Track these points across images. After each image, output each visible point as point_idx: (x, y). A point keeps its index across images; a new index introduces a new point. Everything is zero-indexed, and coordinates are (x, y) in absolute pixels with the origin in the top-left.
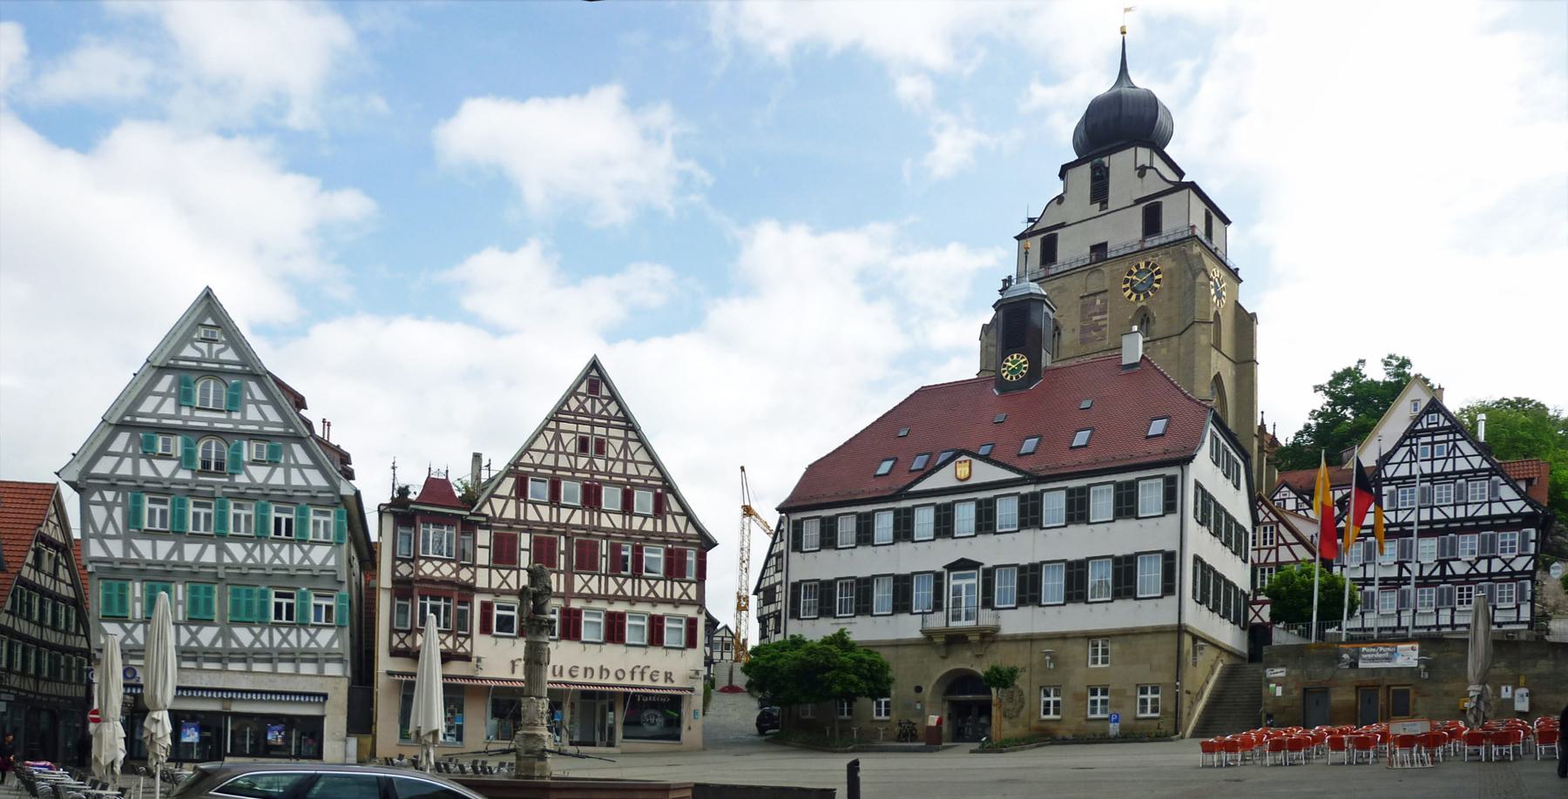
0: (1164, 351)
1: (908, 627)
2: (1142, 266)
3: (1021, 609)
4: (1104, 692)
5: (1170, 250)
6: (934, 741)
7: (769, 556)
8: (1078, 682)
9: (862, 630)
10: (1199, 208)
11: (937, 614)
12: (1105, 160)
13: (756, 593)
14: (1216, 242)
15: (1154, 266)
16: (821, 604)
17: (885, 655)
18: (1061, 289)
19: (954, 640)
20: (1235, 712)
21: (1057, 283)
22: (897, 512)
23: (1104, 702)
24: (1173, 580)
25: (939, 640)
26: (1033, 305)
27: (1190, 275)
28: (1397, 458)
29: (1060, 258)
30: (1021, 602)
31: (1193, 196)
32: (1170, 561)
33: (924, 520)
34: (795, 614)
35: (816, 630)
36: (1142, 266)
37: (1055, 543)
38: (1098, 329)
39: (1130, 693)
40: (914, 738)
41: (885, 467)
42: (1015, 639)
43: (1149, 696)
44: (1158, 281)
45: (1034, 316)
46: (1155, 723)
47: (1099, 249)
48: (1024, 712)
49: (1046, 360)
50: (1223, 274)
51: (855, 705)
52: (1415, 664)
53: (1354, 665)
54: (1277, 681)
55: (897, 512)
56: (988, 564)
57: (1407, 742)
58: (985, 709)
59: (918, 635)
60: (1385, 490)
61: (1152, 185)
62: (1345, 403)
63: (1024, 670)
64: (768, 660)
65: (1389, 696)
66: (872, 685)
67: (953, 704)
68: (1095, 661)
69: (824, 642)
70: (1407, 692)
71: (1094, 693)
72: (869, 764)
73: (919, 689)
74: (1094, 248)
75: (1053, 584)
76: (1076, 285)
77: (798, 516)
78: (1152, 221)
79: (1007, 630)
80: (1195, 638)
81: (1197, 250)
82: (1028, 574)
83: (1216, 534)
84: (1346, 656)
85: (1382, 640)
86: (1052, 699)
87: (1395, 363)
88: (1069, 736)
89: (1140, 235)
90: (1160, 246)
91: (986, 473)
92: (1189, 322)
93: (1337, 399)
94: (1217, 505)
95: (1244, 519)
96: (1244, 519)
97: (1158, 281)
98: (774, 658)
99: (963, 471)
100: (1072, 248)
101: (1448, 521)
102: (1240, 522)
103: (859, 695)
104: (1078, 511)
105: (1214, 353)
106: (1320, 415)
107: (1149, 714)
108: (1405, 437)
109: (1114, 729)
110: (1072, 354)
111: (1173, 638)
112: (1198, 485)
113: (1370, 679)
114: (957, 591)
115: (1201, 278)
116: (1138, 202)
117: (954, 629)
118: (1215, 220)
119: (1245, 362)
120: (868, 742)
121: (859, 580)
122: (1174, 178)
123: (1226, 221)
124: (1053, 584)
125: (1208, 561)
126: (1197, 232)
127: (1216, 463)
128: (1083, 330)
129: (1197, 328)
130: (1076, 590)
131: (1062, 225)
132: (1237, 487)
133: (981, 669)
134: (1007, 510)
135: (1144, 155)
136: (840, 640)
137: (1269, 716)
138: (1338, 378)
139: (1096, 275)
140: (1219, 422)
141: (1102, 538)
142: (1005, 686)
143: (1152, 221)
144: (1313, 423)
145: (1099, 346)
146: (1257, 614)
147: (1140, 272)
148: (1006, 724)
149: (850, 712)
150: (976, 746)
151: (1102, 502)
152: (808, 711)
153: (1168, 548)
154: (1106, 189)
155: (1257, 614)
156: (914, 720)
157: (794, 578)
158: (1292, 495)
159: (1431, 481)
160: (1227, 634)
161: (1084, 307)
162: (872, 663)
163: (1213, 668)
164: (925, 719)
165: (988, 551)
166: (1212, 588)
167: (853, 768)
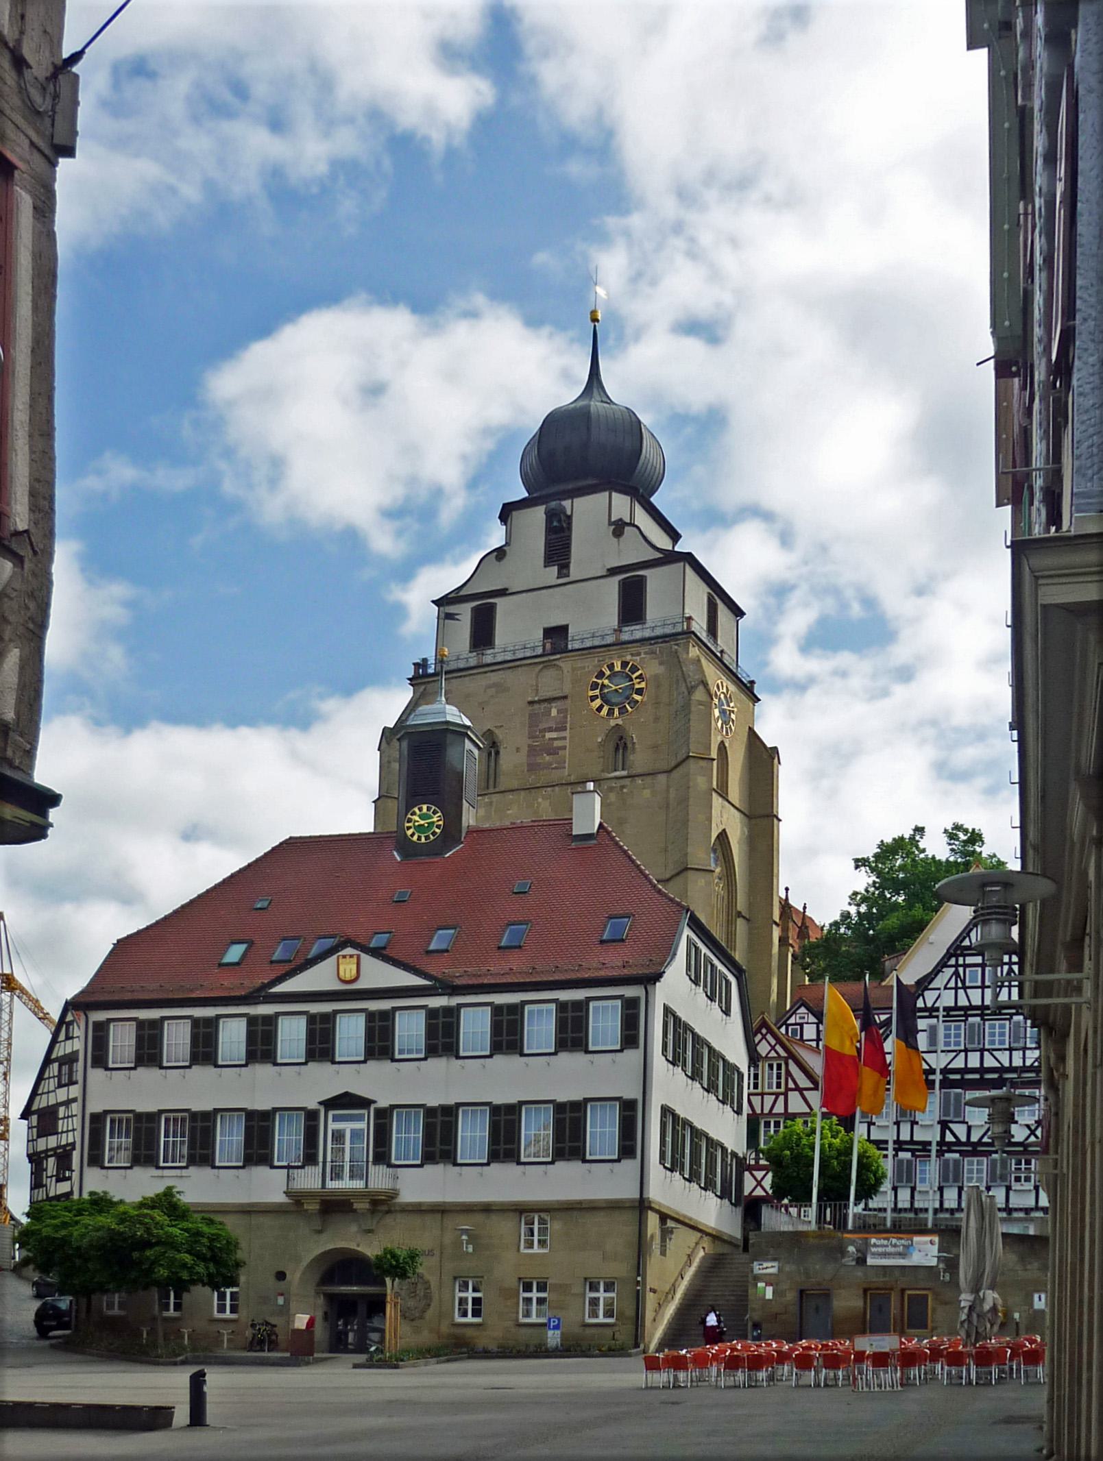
0: (647, 793)
1: (268, 1186)
2: (618, 668)
3: (429, 1168)
4: (542, 1287)
5: (657, 648)
6: (301, 1350)
7: (47, 1061)
8: (506, 1271)
9: (198, 1188)
10: (697, 595)
11: (309, 1169)
12: (567, 504)
13: (25, 1115)
14: (724, 642)
15: (634, 669)
16: (136, 1145)
17: (233, 1226)
18: (500, 688)
19: (334, 1207)
20: (718, 1322)
21: (494, 678)
22: (252, 1021)
23: (541, 1301)
24: (634, 1139)
25: (312, 1206)
26: (450, 737)
27: (684, 689)
28: (939, 982)
29: (498, 640)
30: (429, 1158)
31: (689, 570)
32: (629, 1114)
33: (292, 1034)
34: (95, 1159)
35: (131, 1186)
36: (618, 668)
37: (475, 1081)
38: (553, 751)
39: (577, 1289)
40: (273, 1345)
41: (234, 953)
42: (418, 1210)
43: (601, 1295)
44: (640, 692)
45: (452, 754)
46: (609, 1332)
47: (556, 634)
48: (430, 1313)
49: (470, 818)
50: (732, 688)
51: (186, 1296)
52: (934, 1262)
53: (861, 1261)
54: (768, 1281)
55: (252, 1021)
56: (383, 1103)
57: (880, 1360)
58: (377, 1306)
59: (281, 1198)
60: (922, 1024)
61: (630, 552)
62: (897, 886)
63: (430, 1253)
64: (57, 1228)
65: (901, 1303)
66: (212, 1269)
67: (331, 1298)
68: (530, 1245)
69: (142, 1205)
70: (925, 1297)
71: (528, 1288)
72: (215, 1379)
73: (281, 1276)
74: (549, 632)
75: (472, 1135)
76: (522, 683)
77: (101, 1016)
78: (632, 604)
79: (408, 1196)
80: (664, 1217)
81: (694, 652)
82: (505, 1018)
83: (695, 1076)
84: (851, 1249)
85: (898, 1228)
86: (470, 1295)
87: (962, 837)
88: (493, 1347)
89: (614, 622)
90: (643, 641)
91: (379, 974)
92: (680, 757)
93: (887, 881)
94: (696, 1037)
95: (737, 1055)
96: (737, 1055)
97: (640, 692)
98: (65, 1225)
99: (348, 969)
100: (517, 630)
101: (1001, 1070)
102: (731, 1059)
103: (193, 1282)
104: (507, 1036)
105: (717, 800)
106: (864, 899)
107: (601, 1319)
108: (949, 955)
109: (553, 1338)
110: (515, 784)
111: (632, 1217)
112: (667, 1010)
113: (880, 1280)
114: (338, 1137)
115: (699, 695)
116: (613, 572)
117: (333, 1192)
118: (723, 612)
119: (761, 815)
120: (200, 1353)
121: (139, 1117)
122: (663, 542)
123: (738, 612)
124: (472, 1135)
125: (682, 1113)
126: (694, 627)
127: (696, 982)
128: (532, 751)
129: (692, 765)
130: (504, 1142)
131: (503, 593)
132: (727, 1012)
133: (371, 1249)
134: (410, 1028)
135: (621, 504)
136: (167, 1203)
137: (756, 1326)
138: (888, 851)
139: (550, 673)
140: (696, 925)
141: (540, 1077)
142: (403, 1275)
143: (632, 604)
144: (853, 910)
145: (555, 776)
146: (759, 1183)
147: (614, 675)
148: (405, 1329)
149: (178, 1307)
150: (361, 1358)
151: (540, 1028)
152: (113, 1305)
153: (628, 1095)
154: (567, 546)
155: (759, 1183)
156: (273, 1321)
157: (95, 1107)
158: (812, 1019)
159: (982, 1016)
160: (711, 1211)
161: (534, 720)
162: (214, 1238)
163: (690, 1258)
164: (290, 1319)
165: (382, 1084)
166: (689, 1150)
167: (197, 1383)
